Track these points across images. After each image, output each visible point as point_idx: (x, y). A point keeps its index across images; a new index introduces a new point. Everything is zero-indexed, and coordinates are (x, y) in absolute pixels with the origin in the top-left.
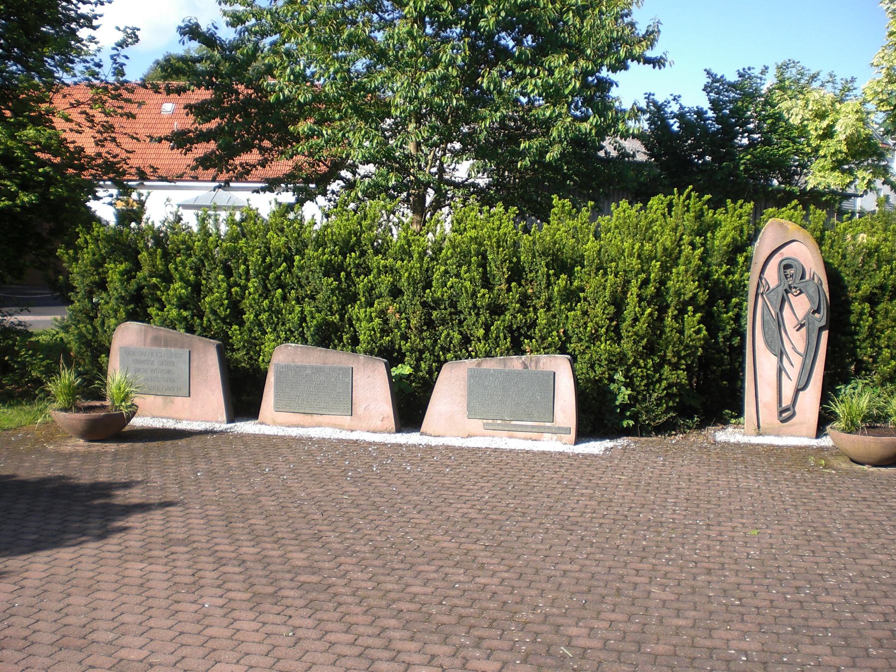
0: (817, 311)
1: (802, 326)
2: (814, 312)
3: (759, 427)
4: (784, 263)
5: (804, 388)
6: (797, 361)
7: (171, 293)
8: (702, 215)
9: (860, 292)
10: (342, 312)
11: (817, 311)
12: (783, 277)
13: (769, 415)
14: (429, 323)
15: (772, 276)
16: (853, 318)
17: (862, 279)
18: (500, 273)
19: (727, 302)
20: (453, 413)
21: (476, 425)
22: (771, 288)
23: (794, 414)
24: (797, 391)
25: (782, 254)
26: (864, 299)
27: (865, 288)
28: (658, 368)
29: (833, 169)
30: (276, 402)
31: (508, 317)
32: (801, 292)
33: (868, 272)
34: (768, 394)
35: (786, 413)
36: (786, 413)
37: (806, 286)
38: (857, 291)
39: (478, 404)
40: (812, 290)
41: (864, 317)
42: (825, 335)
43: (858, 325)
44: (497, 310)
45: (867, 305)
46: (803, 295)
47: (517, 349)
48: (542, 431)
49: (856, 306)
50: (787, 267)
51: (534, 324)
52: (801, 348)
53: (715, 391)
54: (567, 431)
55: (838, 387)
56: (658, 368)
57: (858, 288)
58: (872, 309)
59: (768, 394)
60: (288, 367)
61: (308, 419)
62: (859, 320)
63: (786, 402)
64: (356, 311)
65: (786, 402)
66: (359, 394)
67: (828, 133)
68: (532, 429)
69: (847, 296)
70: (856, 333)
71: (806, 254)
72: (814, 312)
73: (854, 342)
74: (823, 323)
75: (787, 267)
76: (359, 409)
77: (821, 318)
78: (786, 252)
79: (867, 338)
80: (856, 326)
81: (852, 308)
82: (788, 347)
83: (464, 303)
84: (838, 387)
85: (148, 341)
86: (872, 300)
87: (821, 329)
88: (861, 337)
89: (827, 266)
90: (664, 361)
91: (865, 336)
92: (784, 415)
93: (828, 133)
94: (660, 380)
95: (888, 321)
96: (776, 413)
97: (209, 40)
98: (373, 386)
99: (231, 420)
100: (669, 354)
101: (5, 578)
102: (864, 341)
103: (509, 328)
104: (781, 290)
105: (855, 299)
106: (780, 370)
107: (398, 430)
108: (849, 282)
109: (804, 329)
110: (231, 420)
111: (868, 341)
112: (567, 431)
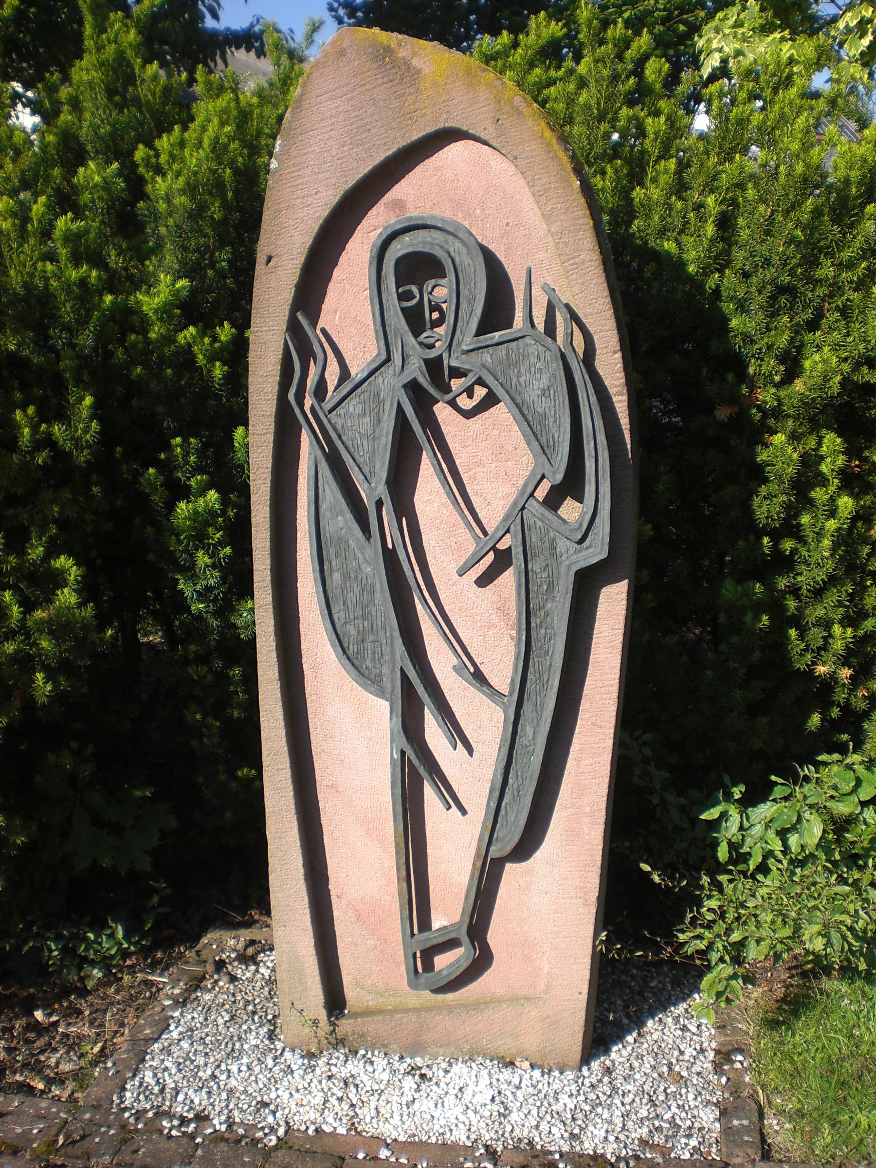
0: (571, 485)
1: (503, 560)
2: (553, 501)
3: (335, 1001)
4: (398, 249)
5: (527, 846)
6: (484, 720)
8: (130, 79)
9: (799, 386)
11: (571, 485)
12: (397, 321)
15: (351, 312)
16: (767, 506)
17: (813, 325)
22: (357, 370)
23: (482, 961)
25: (399, 205)
26: (821, 415)
27: (822, 363)
32: (490, 401)
33: (836, 289)
34: (363, 867)
36: (456, 952)
37: (510, 363)
38: (789, 378)
40: (540, 382)
41: (819, 494)
42: (613, 603)
43: (789, 528)
45: (831, 441)
46: (501, 412)
49: (780, 451)
52: (502, 672)
55: (712, 814)
57: (792, 364)
58: (852, 451)
59: (363, 867)
62: (792, 511)
63: (448, 911)
65: (448, 911)
69: (742, 406)
70: (786, 563)
72: (553, 501)
73: (774, 605)
74: (596, 551)
77: (585, 527)
78: (415, 194)
79: (832, 580)
80: (776, 536)
81: (763, 456)
84: (712, 814)
87: (587, 585)
88: (805, 579)
89: (632, 268)
91: (821, 576)
92: (441, 961)
102: (818, 593)
104: (390, 386)
105: (777, 413)
108: (749, 339)
109: (508, 579)
111: (832, 597)
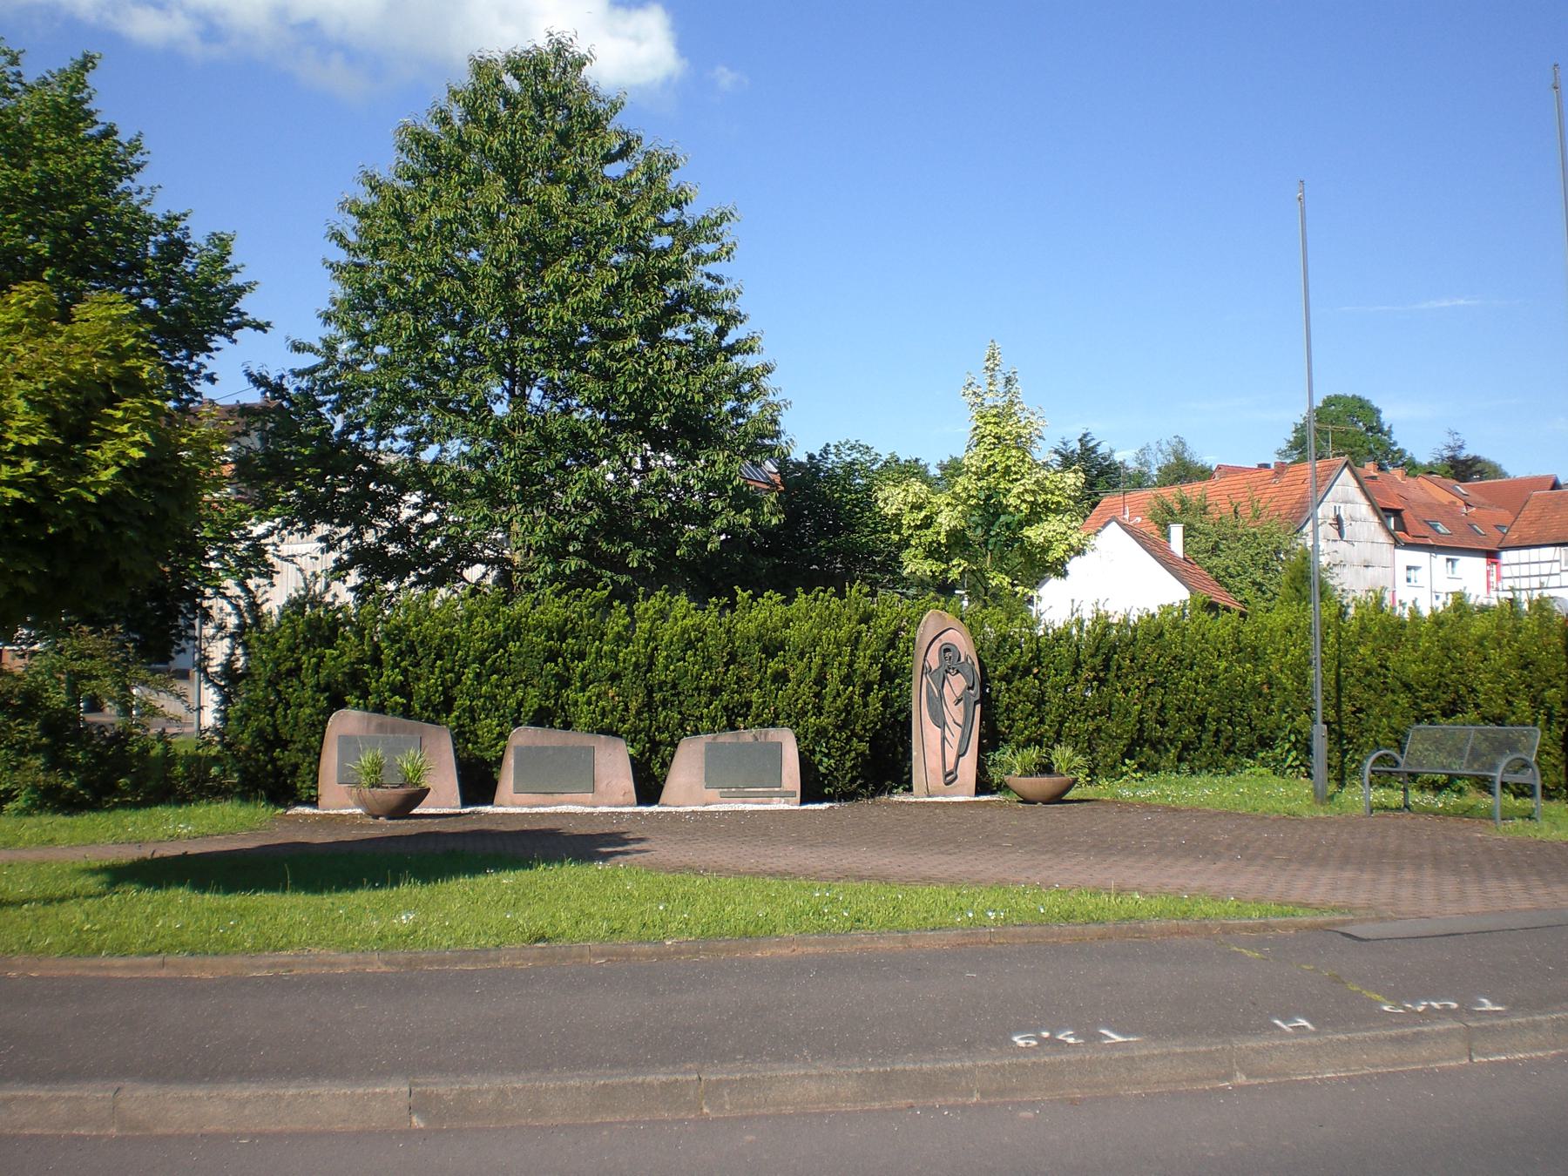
0: (971, 688)
6: (957, 731)
7: (384, 679)
10: (558, 696)
13: (937, 780)
14: (649, 705)
15: (934, 659)
18: (720, 659)
19: (892, 682)
20: (689, 781)
21: (714, 793)
24: (959, 756)
27: (1001, 669)
28: (849, 739)
29: (926, 558)
30: (515, 785)
31: (725, 696)
34: (934, 762)
35: (950, 777)
36: (950, 777)
39: (717, 774)
40: (967, 670)
44: (715, 691)
47: (732, 727)
48: (771, 795)
50: (947, 650)
51: (748, 704)
53: (883, 762)
54: (793, 794)
56: (849, 739)
60: (529, 748)
61: (549, 797)
64: (570, 694)
66: (600, 770)
67: (927, 523)
68: (763, 795)
71: (959, 638)
75: (947, 650)
76: (601, 786)
82: (949, 720)
83: (686, 686)
85: (372, 728)
86: (1006, 678)
90: (854, 734)
93: (927, 523)
94: (849, 752)
95: (1021, 697)
96: (942, 777)
97: (278, 390)
98: (614, 764)
99: (465, 804)
100: (858, 728)
101: (605, 857)
103: (725, 708)
104: (942, 670)
106: (944, 739)
107: (640, 803)
110: (465, 804)
112: (793, 794)
